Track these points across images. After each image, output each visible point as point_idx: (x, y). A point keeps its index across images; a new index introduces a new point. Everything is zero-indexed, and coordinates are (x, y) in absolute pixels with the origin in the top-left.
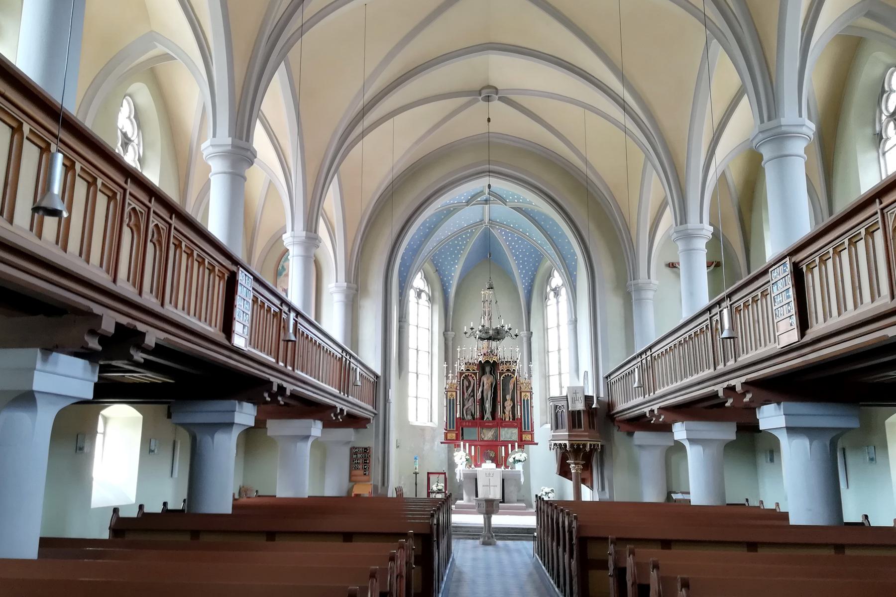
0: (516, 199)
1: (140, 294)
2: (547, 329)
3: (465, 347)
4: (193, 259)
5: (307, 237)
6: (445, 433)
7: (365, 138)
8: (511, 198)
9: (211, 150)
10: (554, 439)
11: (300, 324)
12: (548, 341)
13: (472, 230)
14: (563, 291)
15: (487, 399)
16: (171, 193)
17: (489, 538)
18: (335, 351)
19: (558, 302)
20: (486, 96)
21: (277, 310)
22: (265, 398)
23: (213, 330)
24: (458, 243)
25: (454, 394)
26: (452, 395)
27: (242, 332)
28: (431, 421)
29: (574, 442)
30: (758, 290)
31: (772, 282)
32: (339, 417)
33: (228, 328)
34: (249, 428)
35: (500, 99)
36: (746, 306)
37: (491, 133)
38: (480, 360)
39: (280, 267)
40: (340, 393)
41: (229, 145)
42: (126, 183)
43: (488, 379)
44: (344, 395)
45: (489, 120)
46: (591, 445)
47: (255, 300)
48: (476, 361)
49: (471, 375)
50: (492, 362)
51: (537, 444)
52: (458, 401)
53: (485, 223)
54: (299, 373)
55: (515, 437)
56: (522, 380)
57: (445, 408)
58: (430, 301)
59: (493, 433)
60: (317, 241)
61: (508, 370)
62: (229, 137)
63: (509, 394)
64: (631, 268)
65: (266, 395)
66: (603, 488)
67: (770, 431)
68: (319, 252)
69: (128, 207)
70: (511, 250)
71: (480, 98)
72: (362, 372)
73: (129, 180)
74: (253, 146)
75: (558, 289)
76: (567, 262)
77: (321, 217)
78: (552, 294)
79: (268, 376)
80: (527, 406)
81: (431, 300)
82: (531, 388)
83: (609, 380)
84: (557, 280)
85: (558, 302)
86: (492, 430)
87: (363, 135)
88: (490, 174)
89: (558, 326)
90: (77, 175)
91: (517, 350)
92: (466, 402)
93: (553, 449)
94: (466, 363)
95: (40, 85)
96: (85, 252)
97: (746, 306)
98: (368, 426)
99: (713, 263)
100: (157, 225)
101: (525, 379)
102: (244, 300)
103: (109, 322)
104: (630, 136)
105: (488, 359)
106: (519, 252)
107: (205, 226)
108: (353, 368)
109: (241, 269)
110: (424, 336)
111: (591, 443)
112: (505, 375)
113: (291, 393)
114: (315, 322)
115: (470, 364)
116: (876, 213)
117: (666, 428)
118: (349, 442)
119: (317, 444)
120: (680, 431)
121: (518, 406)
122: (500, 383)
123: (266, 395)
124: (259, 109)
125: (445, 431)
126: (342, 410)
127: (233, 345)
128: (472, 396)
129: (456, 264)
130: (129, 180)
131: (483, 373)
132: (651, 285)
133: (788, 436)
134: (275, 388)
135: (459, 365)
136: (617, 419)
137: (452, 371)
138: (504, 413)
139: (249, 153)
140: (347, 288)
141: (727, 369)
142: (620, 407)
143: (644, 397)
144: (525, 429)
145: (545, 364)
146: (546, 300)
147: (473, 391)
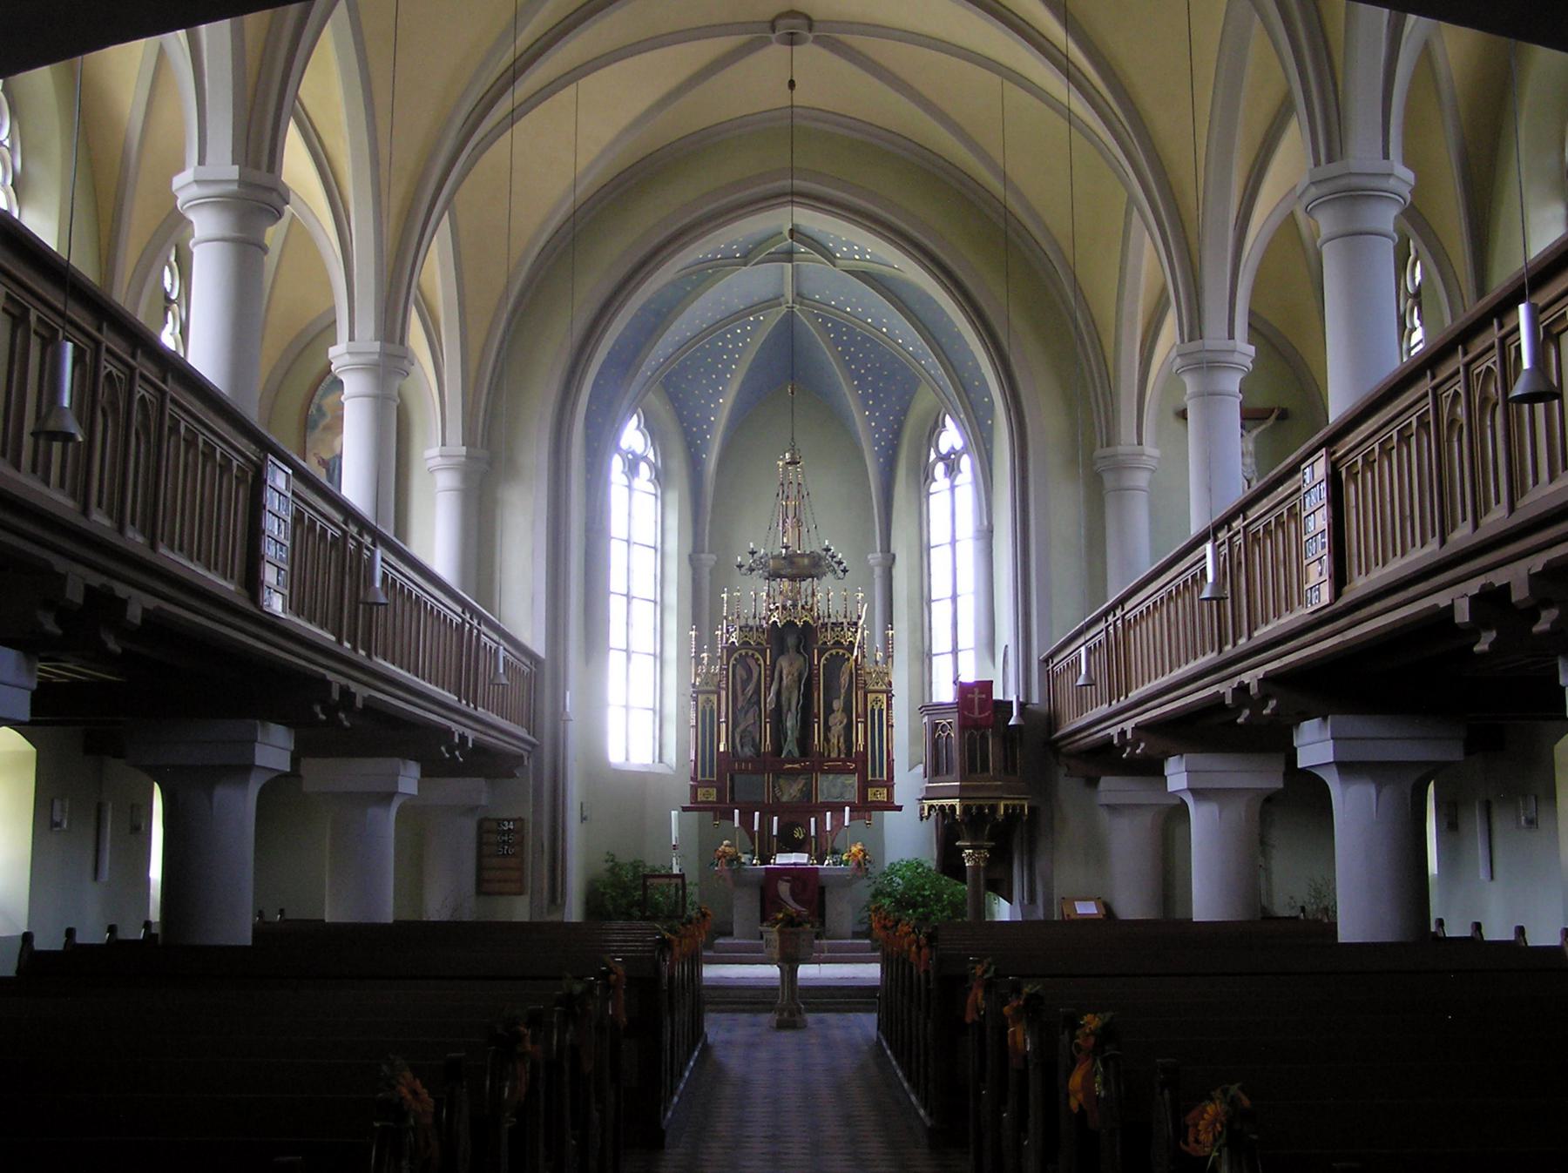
0: (856, 252)
2: (929, 548)
3: (738, 591)
5: (384, 354)
6: (692, 786)
7: (518, 123)
8: (845, 249)
9: (195, 191)
10: (929, 796)
11: (484, 634)
12: (929, 575)
13: (757, 319)
14: (966, 462)
15: (789, 710)
16: (84, 264)
17: (791, 1014)
18: (448, 611)
19: (953, 488)
20: (787, 33)
21: (338, 533)
22: (317, 715)
23: (227, 586)
24: (725, 345)
25: (714, 698)
26: (708, 701)
27: (275, 583)
28: (661, 761)
29: (971, 802)
30: (1283, 505)
31: (1304, 491)
32: (457, 753)
33: (253, 583)
34: (280, 776)
35: (818, 41)
37: (797, 107)
38: (773, 619)
39: (313, 409)
40: (460, 701)
43: (791, 665)
44: (468, 705)
45: (792, 84)
46: (1006, 807)
47: (298, 518)
48: (764, 622)
49: (753, 655)
50: (800, 624)
51: (899, 808)
52: (723, 714)
53: (788, 303)
54: (381, 663)
55: (852, 795)
56: (869, 666)
57: (692, 731)
58: (658, 481)
59: (800, 786)
60: (406, 362)
61: (838, 644)
62: (234, 163)
63: (839, 698)
64: (1103, 423)
65: (318, 709)
66: (1032, 899)
67: (1311, 770)
68: (408, 384)
70: (848, 364)
71: (773, 36)
72: (511, 658)
73: (105, 325)
74: (282, 179)
75: (953, 456)
76: (972, 395)
77: (414, 308)
78: (940, 469)
79: (321, 670)
80: (879, 723)
81: (661, 478)
82: (890, 684)
83: (1051, 665)
84: (951, 437)
85: (953, 488)
86: (799, 779)
87: (513, 117)
88: (795, 199)
89: (953, 542)
91: (860, 597)
92: (740, 717)
93: (927, 818)
94: (741, 628)
95: (223, 390)
99: (1273, 411)
100: (143, 397)
101: (877, 662)
102: (279, 518)
103: (78, 580)
105: (788, 619)
106: (867, 370)
107: (156, 333)
108: (486, 644)
110: (645, 563)
111: (1008, 802)
112: (831, 654)
113: (364, 705)
114: (394, 539)
115: (751, 628)
116: (1426, 395)
117: (1152, 769)
118: (473, 809)
119: (412, 814)
121: (859, 725)
122: (819, 673)
123: (318, 709)
124: (296, 96)
125: (692, 783)
126: (463, 738)
128: (755, 703)
129: (721, 395)
130: (105, 325)
131: (780, 650)
132: (1144, 458)
133: (1340, 778)
134: (336, 696)
135: (725, 631)
136: (1064, 750)
137: (709, 647)
138: (827, 740)
139: (275, 195)
141: (1238, 650)
142: (1071, 723)
143: (1110, 705)
144: (874, 775)
145: (923, 630)
146: (926, 480)
147: (757, 691)
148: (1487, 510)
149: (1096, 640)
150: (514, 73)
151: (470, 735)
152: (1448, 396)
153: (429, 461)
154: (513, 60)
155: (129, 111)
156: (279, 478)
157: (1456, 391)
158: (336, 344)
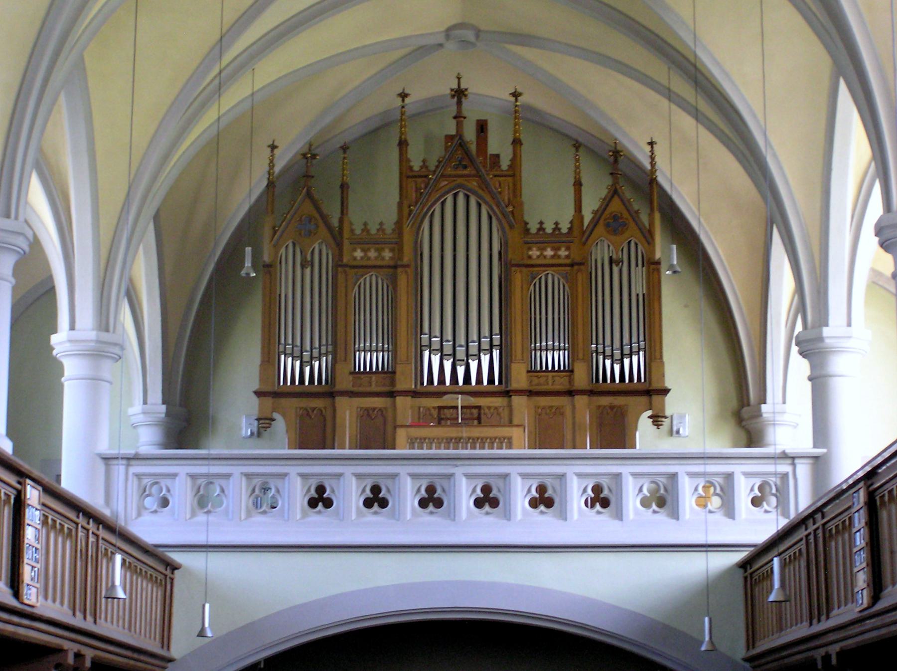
41: (162, 413)
83: (749, 571)
127: (22, 603)
148: (833, 609)
149: (796, 549)
150: (220, 83)
153: (132, 418)
154: (218, 37)
156: (32, 494)
158: (56, 333)
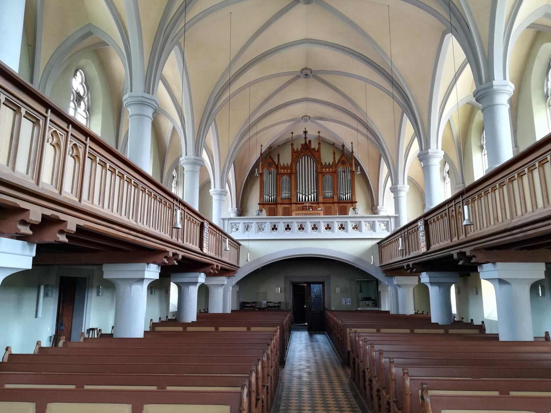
1: (183, 242)
4: (116, 174)
33: (201, 247)
36: (434, 221)
40: (216, 255)
42: (217, 231)
69: (70, 145)
73: (175, 200)
90: (23, 116)
96: (119, 209)
97: (438, 219)
98: (235, 275)
104: (396, 101)
108: (224, 240)
109: (205, 221)
120: (425, 278)
126: (217, 266)
140: (237, 210)
151: (220, 265)
152: (458, 207)
155: (122, 90)
157: (460, 206)
